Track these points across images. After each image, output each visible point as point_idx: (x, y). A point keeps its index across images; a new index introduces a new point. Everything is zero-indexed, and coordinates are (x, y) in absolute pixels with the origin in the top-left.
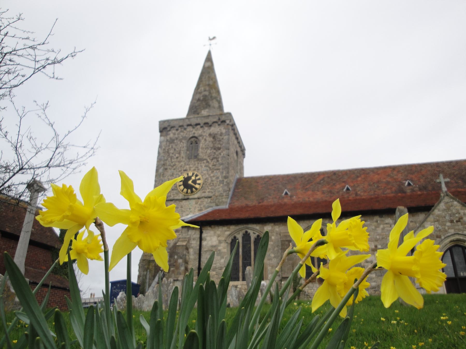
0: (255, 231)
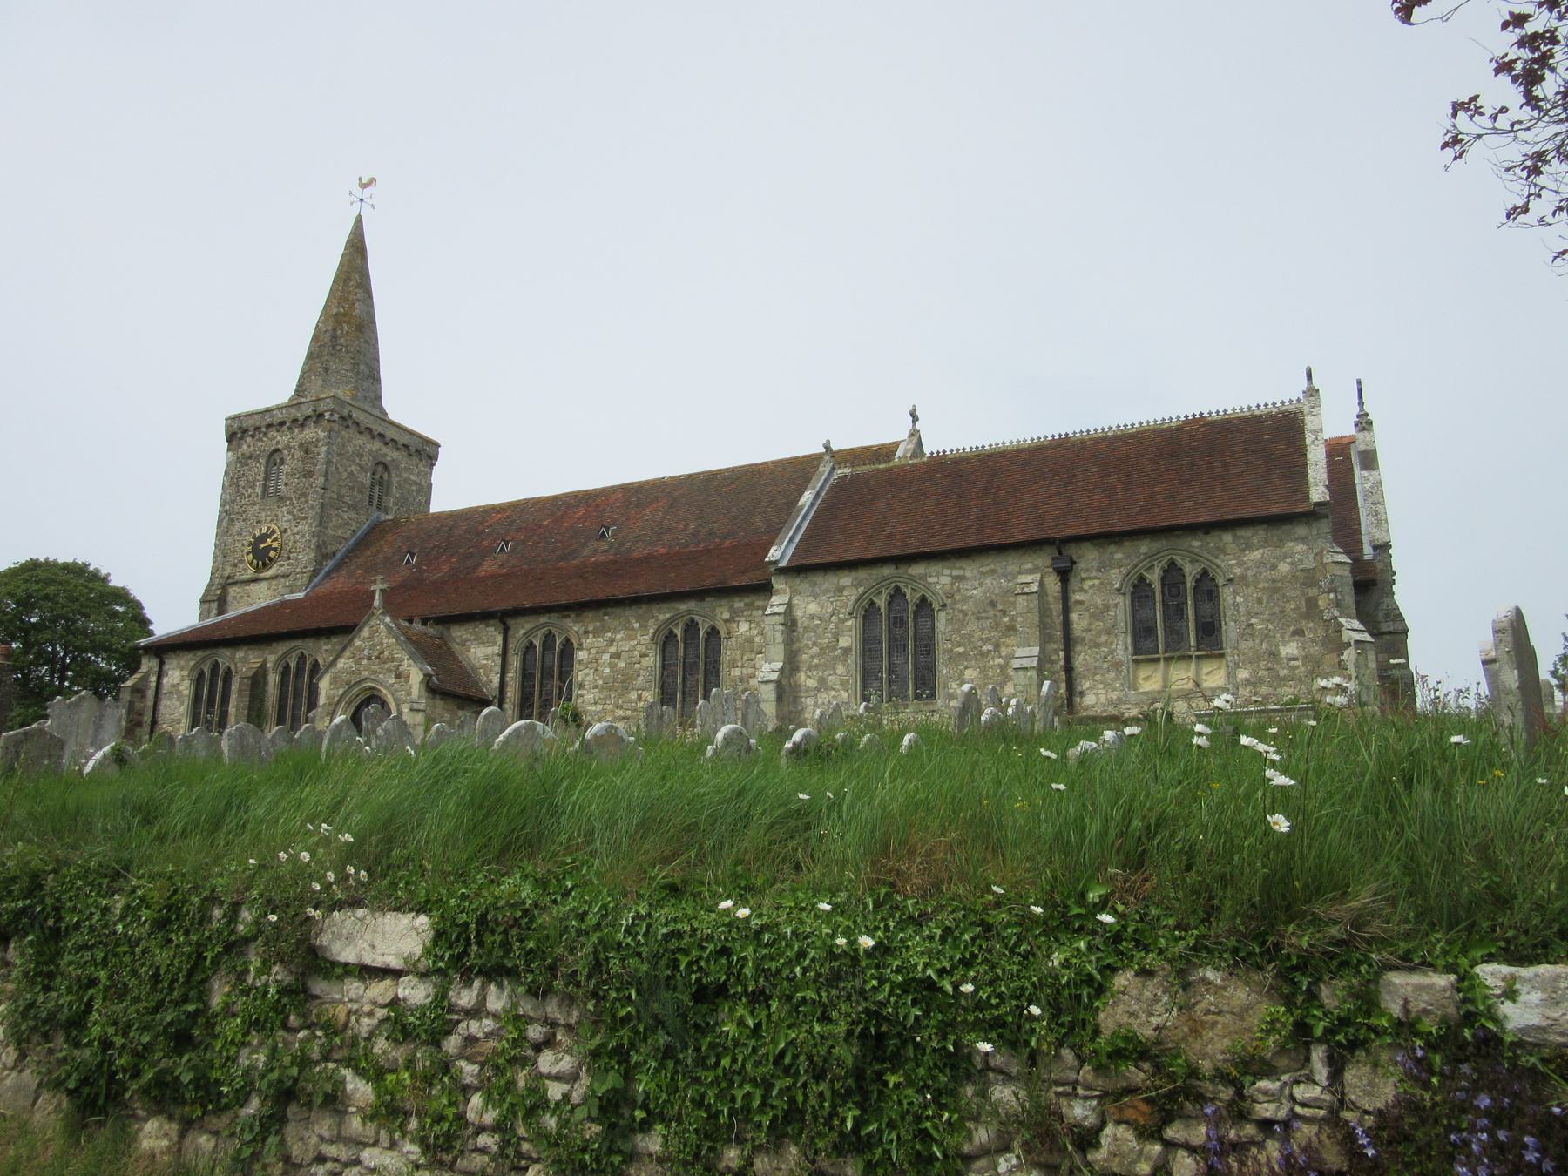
0: (224, 657)
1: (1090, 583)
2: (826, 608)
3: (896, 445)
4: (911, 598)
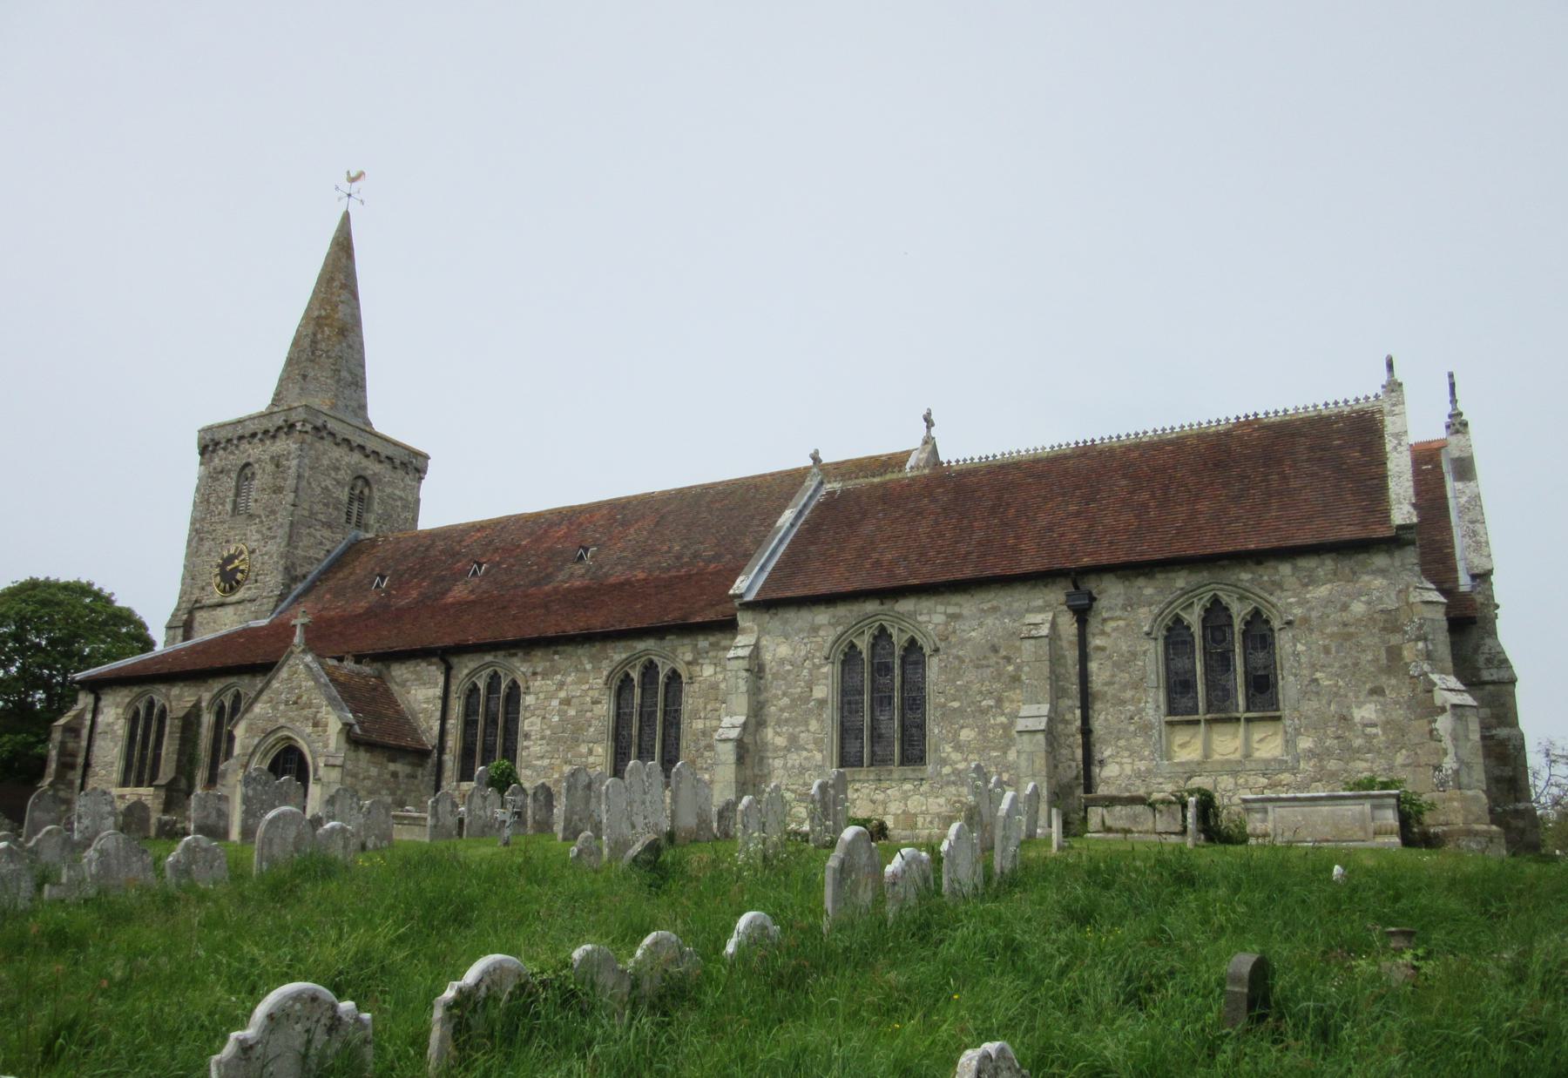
1: (1113, 624)
2: (799, 653)
3: (908, 453)
4: (899, 640)
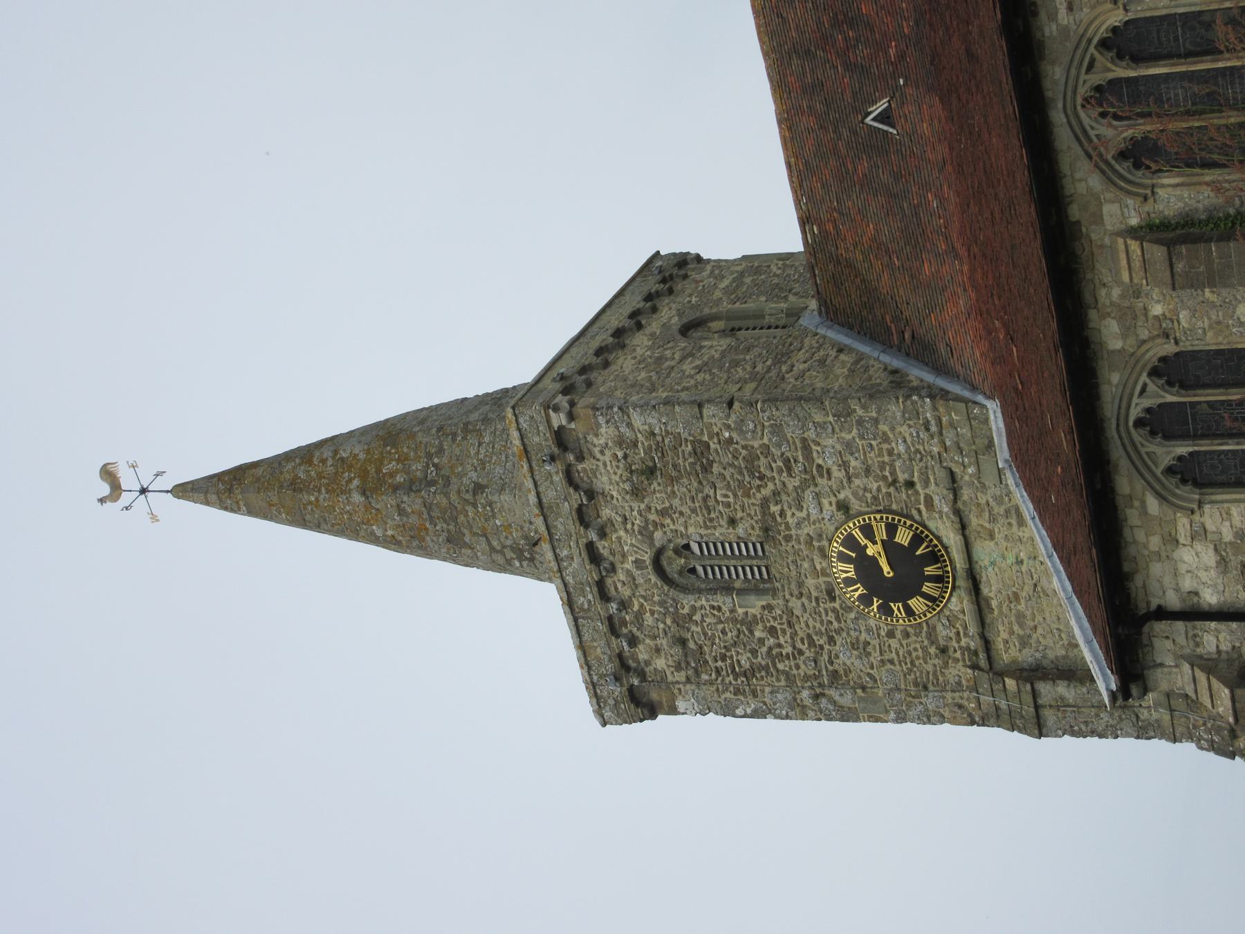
0: (1127, 393)
